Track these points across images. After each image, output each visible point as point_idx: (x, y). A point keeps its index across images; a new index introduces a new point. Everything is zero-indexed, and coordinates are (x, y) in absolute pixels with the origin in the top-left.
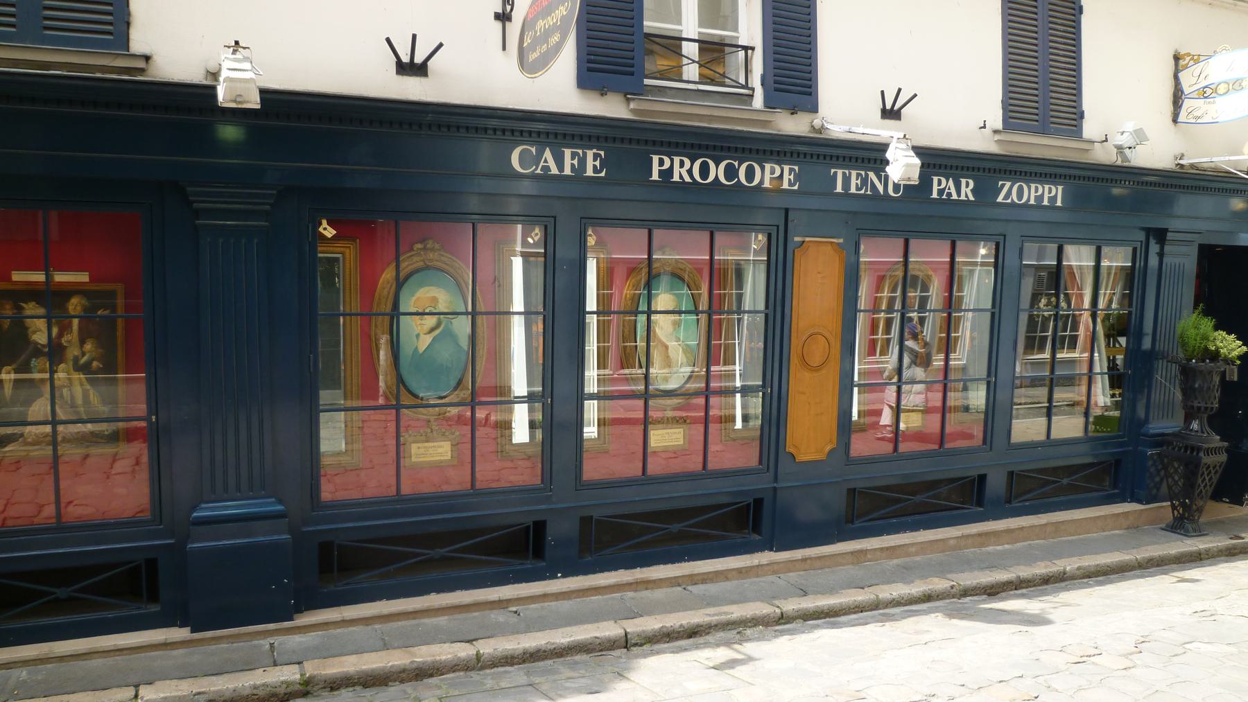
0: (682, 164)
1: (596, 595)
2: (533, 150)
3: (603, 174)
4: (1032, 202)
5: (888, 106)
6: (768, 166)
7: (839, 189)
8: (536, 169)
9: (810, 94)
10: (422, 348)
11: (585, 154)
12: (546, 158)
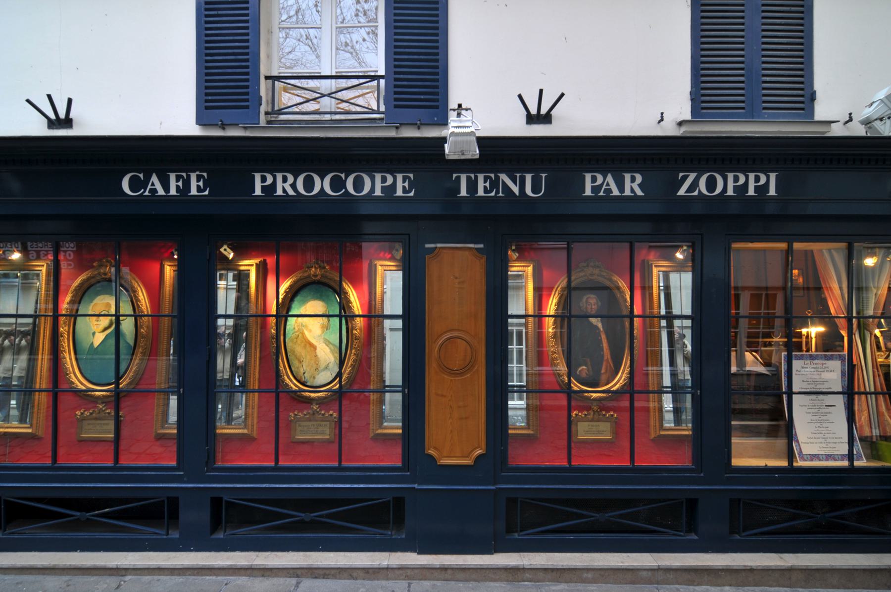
0: (285, 180)
1: (211, 575)
2: (141, 176)
3: (412, 194)
5: (534, 111)
6: (730, 176)
7: (463, 192)
8: (144, 192)
10: (96, 344)
11: (189, 177)
12: (608, 182)
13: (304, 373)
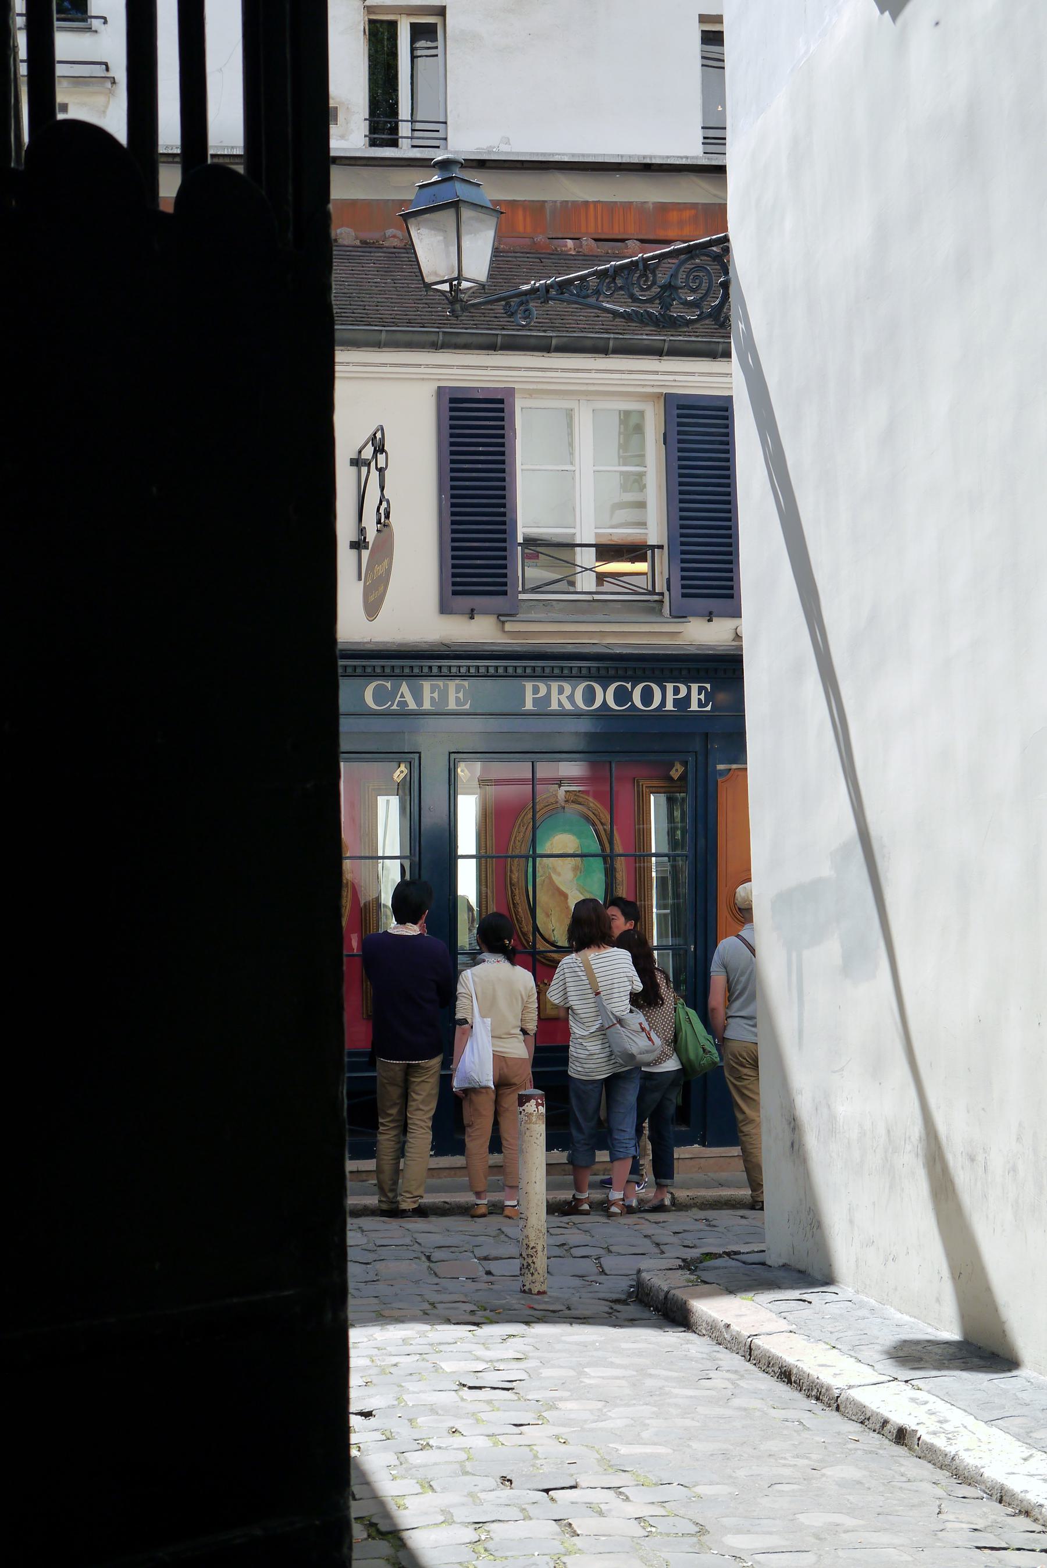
0: (561, 691)
3: (709, 708)
4: (669, 706)
6: (670, 687)
9: (731, 596)
11: (446, 687)
13: (553, 931)
